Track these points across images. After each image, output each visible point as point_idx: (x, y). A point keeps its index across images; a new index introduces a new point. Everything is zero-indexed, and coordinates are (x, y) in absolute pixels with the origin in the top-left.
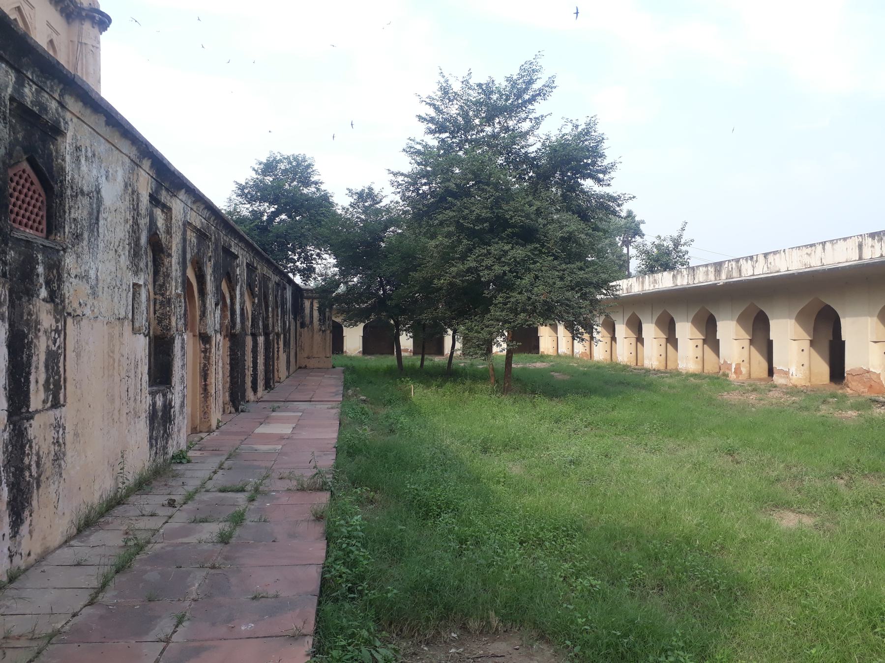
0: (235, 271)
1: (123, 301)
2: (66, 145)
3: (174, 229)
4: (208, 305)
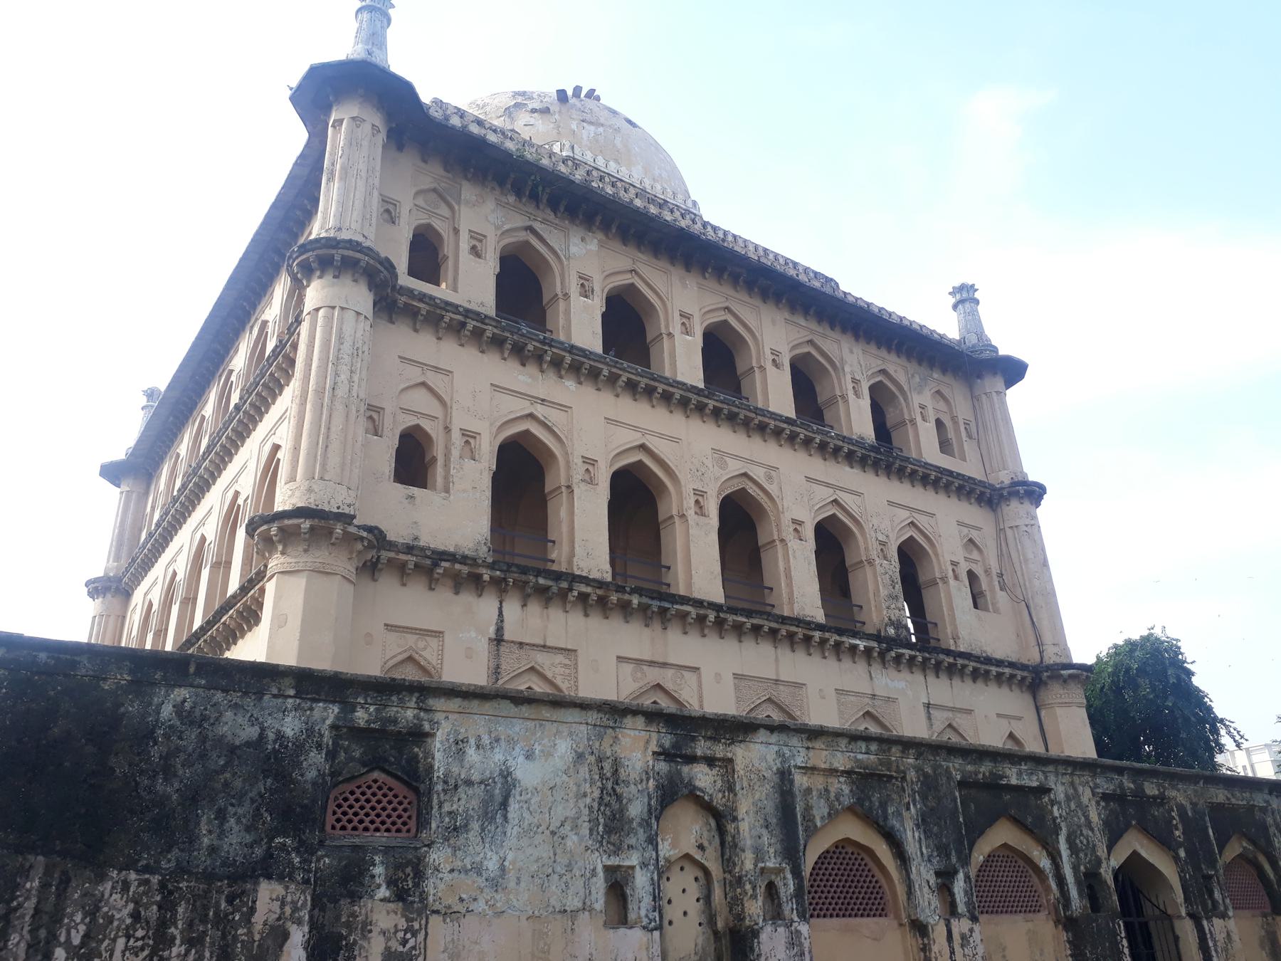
4: (914, 876)
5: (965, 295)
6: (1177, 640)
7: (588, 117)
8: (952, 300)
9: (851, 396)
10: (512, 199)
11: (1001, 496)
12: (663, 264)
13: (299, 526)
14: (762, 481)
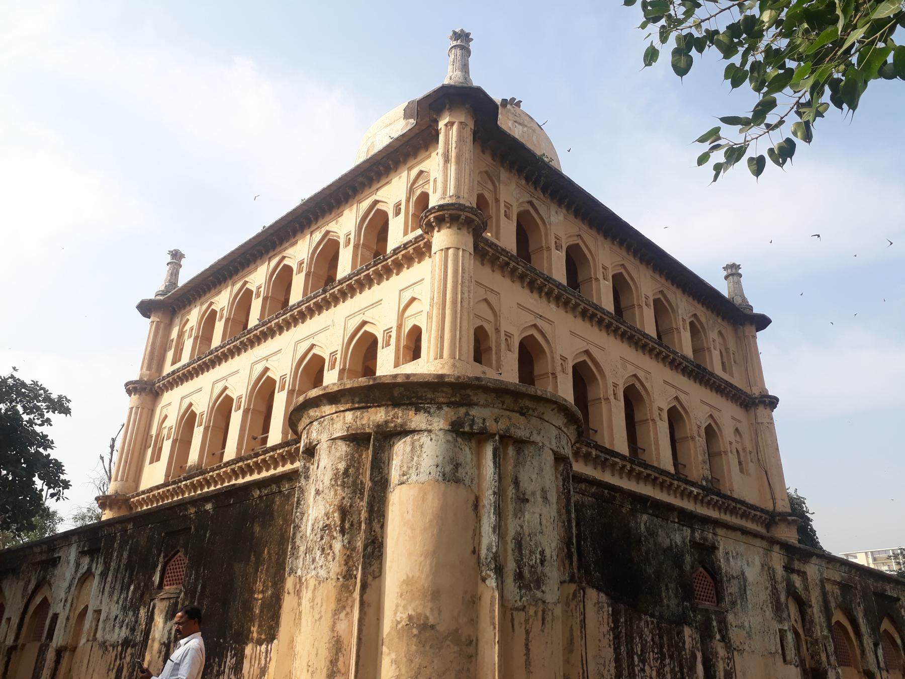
2: (720, 554)
5: (734, 271)
6: (69, 401)
7: (518, 119)
8: (725, 273)
9: (682, 330)
10: (523, 182)
12: (594, 232)
14: (643, 380)
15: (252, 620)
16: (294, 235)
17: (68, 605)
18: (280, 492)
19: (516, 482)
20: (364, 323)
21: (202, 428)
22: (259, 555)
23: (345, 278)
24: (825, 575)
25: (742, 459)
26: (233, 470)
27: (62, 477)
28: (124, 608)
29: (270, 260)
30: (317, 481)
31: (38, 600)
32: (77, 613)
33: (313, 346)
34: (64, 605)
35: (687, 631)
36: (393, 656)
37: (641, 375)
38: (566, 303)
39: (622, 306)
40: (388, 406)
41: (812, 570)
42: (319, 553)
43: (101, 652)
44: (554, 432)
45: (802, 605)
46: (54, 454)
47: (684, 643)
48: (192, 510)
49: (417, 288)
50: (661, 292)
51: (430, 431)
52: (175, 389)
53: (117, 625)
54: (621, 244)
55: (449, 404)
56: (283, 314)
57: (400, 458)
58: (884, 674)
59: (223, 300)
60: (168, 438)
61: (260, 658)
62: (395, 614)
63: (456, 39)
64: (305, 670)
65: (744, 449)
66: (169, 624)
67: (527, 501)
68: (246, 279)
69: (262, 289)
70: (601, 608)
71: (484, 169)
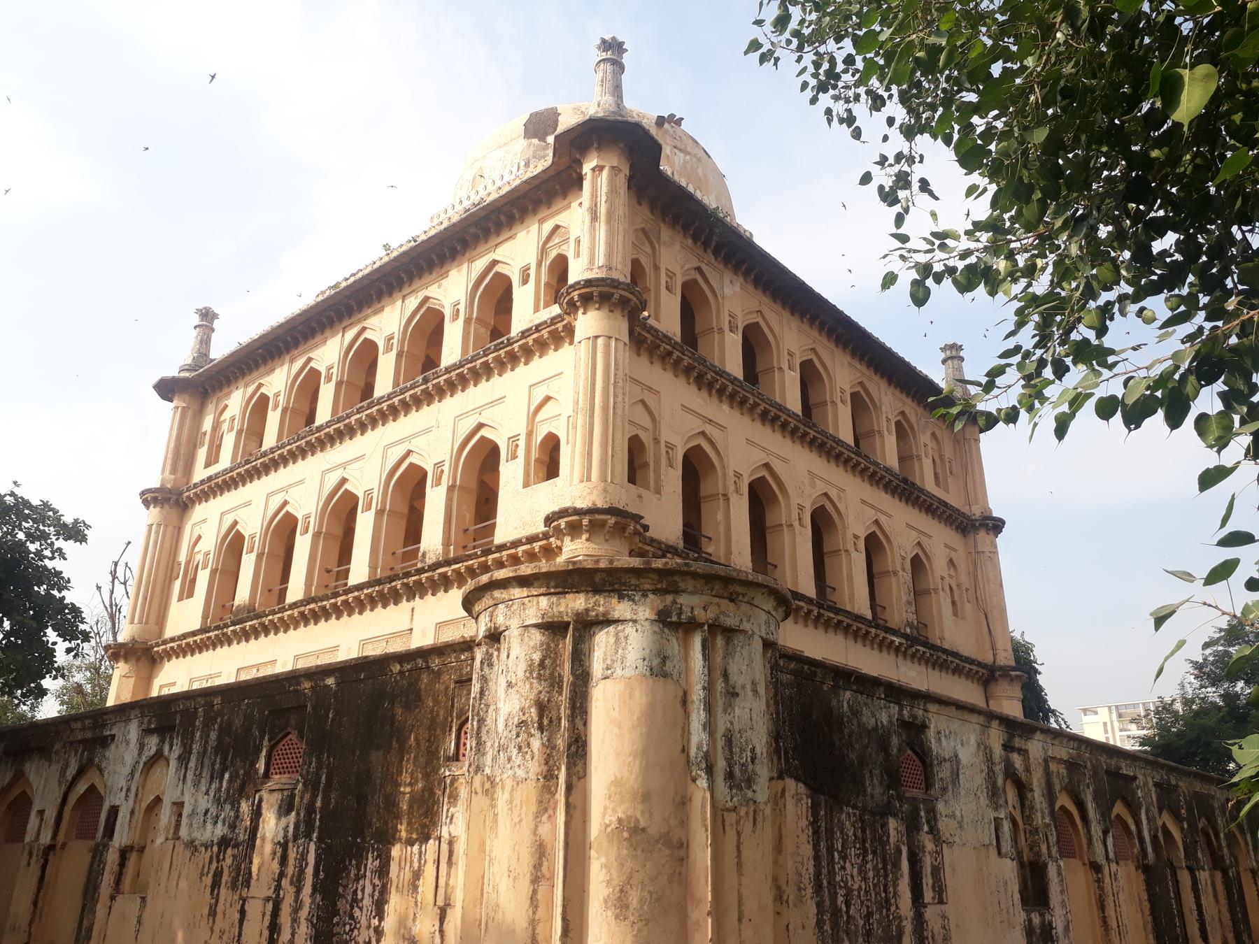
0: (1134, 794)
1: (986, 831)
2: (931, 733)
3: (1033, 767)
4: (1093, 833)
5: (954, 353)
6: (88, 527)
7: (679, 144)
8: (943, 356)
10: (690, 242)
11: (973, 526)
12: (778, 307)
13: (605, 521)
15: (398, 817)
16: (379, 299)
17: (132, 795)
18: (428, 668)
19: (726, 675)
20: (481, 426)
21: (253, 556)
22: (402, 743)
23: (455, 365)
24: (1050, 753)
25: (956, 598)
26: (302, 614)
27: (82, 627)
28: (217, 801)
29: (344, 330)
30: (508, 672)
31: (82, 787)
32: (144, 805)
33: (409, 453)
34: (127, 796)
35: (892, 823)
36: (603, 860)
37: (833, 494)
38: (742, 403)
39: (811, 402)
40: (588, 592)
41: (1036, 747)
42: (515, 751)
43: (188, 853)
44: (764, 616)
45: (1022, 788)
46: (70, 597)
47: (888, 837)
48: (307, 685)
49: (554, 384)
50: (861, 383)
51: (635, 621)
52: (212, 501)
53: (209, 821)
54: (812, 322)
55: (655, 591)
56: (364, 408)
57: (603, 650)
58: (1114, 866)
59: (277, 381)
60: (205, 567)
61: (411, 861)
62: (604, 816)
63: (606, 50)
64: (506, 874)
65: (959, 586)
66: (284, 821)
67: (737, 695)
68: (311, 355)
69: (334, 370)
70: (800, 800)
71: (641, 226)
